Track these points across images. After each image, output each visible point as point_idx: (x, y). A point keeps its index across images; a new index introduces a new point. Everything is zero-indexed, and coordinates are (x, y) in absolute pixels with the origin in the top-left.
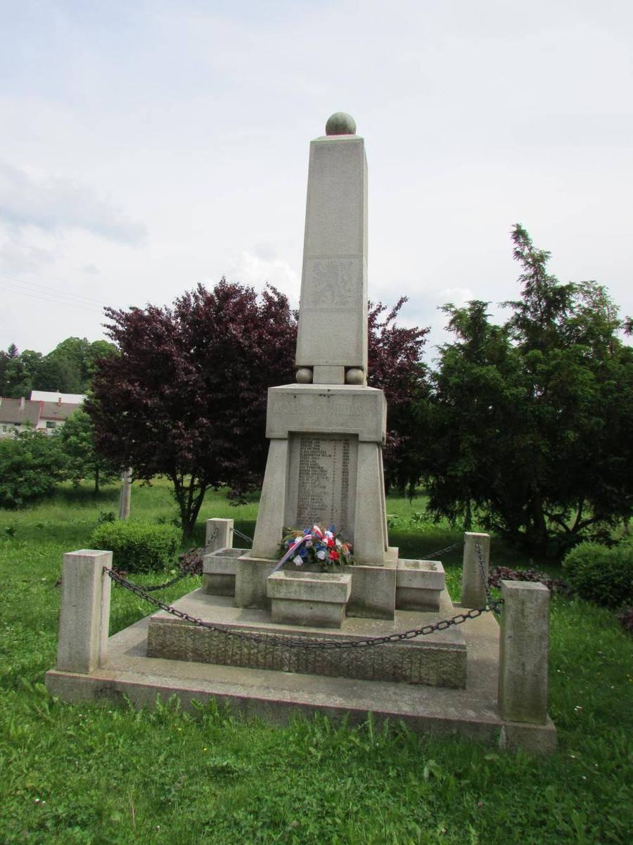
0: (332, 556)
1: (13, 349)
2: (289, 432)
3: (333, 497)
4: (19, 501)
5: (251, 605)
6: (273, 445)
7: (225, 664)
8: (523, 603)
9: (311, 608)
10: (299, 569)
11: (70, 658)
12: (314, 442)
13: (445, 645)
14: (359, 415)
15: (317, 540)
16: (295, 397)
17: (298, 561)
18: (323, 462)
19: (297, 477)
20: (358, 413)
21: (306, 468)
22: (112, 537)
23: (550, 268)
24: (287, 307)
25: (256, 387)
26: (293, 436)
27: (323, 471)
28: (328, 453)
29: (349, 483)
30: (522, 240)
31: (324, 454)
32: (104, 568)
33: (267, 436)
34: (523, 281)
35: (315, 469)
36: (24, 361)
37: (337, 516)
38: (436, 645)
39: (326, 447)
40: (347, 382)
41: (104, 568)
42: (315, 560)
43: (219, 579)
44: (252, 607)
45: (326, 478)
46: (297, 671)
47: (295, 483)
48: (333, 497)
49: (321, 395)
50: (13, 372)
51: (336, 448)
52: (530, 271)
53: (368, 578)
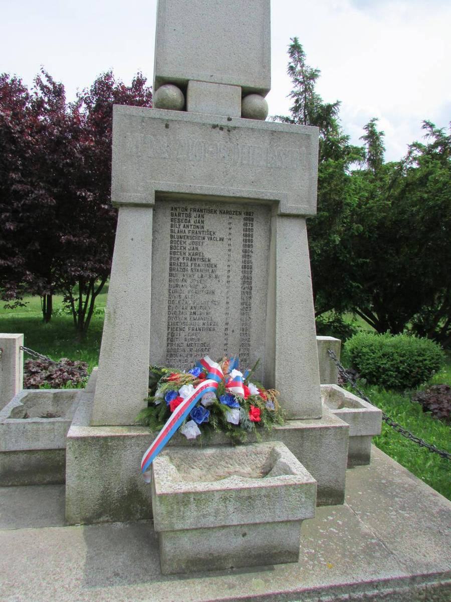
0: (252, 417)
2: (157, 192)
3: (227, 308)
5: (100, 515)
6: (125, 218)
9: (244, 535)
10: (194, 444)
12: (194, 214)
14: (280, 168)
15: (223, 389)
16: (167, 126)
17: (192, 431)
18: (211, 251)
20: (279, 164)
21: (181, 260)
24: (63, 98)
25: (29, 179)
26: (164, 201)
27: (211, 266)
28: (218, 235)
29: (253, 285)
30: (296, 56)
31: (211, 236)
33: (113, 198)
34: (293, 97)
35: (198, 262)
37: (234, 339)
39: (214, 223)
42: (224, 425)
43: (22, 458)
44: (101, 519)
45: (216, 277)
48: (227, 308)
49: (214, 127)
51: (233, 226)
52: (300, 88)
53: (307, 444)
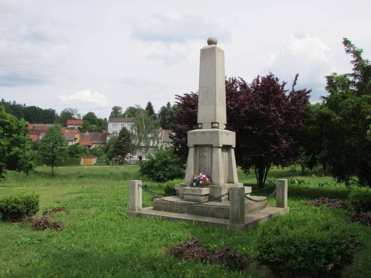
1: (169, 104)
4: (165, 179)
6: (190, 149)
7: (171, 212)
8: (233, 191)
11: (132, 208)
13: (225, 206)
18: (205, 154)
19: (198, 159)
22: (171, 185)
23: (364, 56)
26: (196, 146)
27: (205, 157)
32: (139, 184)
33: (188, 146)
34: (353, 63)
36: (174, 110)
38: (223, 206)
40: (212, 128)
41: (139, 184)
46: (188, 214)
47: (198, 161)
49: (202, 133)
50: (169, 116)
53: (214, 189)
